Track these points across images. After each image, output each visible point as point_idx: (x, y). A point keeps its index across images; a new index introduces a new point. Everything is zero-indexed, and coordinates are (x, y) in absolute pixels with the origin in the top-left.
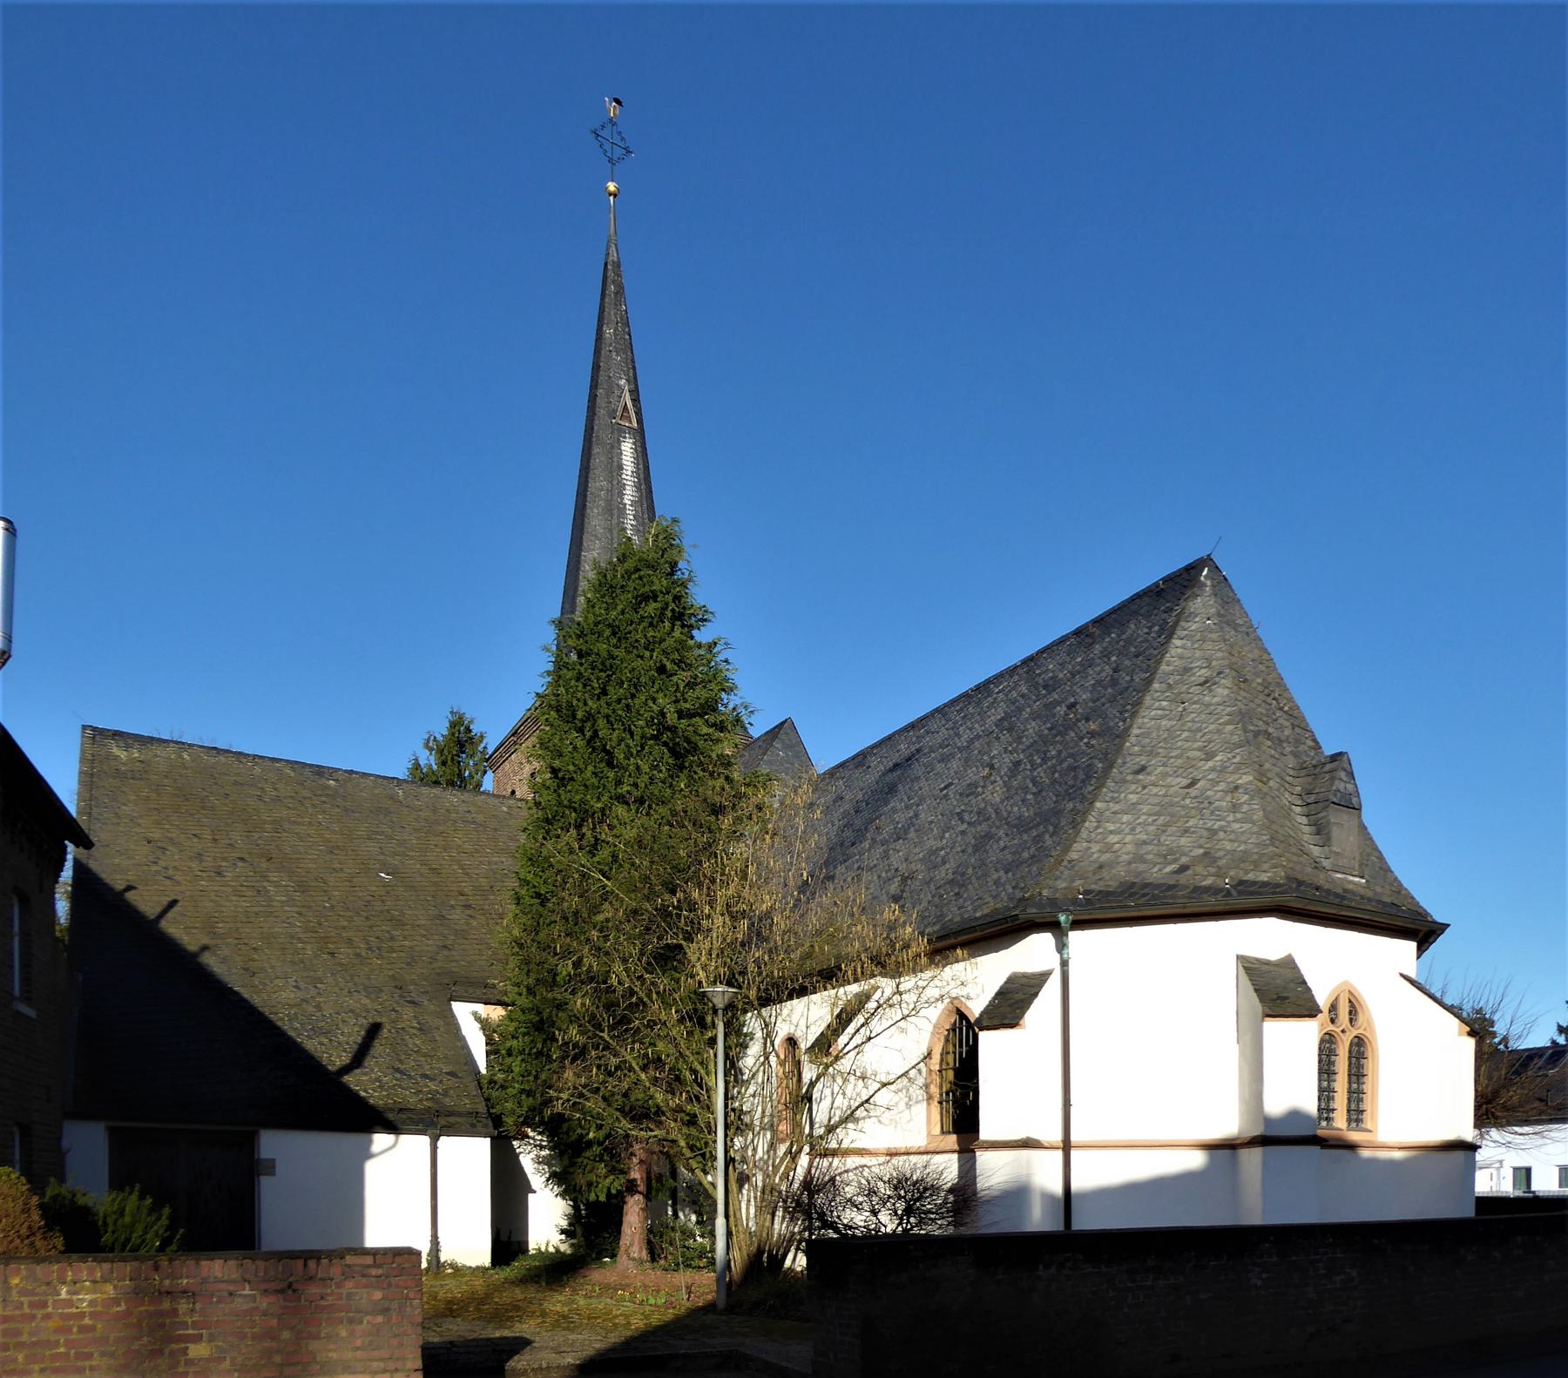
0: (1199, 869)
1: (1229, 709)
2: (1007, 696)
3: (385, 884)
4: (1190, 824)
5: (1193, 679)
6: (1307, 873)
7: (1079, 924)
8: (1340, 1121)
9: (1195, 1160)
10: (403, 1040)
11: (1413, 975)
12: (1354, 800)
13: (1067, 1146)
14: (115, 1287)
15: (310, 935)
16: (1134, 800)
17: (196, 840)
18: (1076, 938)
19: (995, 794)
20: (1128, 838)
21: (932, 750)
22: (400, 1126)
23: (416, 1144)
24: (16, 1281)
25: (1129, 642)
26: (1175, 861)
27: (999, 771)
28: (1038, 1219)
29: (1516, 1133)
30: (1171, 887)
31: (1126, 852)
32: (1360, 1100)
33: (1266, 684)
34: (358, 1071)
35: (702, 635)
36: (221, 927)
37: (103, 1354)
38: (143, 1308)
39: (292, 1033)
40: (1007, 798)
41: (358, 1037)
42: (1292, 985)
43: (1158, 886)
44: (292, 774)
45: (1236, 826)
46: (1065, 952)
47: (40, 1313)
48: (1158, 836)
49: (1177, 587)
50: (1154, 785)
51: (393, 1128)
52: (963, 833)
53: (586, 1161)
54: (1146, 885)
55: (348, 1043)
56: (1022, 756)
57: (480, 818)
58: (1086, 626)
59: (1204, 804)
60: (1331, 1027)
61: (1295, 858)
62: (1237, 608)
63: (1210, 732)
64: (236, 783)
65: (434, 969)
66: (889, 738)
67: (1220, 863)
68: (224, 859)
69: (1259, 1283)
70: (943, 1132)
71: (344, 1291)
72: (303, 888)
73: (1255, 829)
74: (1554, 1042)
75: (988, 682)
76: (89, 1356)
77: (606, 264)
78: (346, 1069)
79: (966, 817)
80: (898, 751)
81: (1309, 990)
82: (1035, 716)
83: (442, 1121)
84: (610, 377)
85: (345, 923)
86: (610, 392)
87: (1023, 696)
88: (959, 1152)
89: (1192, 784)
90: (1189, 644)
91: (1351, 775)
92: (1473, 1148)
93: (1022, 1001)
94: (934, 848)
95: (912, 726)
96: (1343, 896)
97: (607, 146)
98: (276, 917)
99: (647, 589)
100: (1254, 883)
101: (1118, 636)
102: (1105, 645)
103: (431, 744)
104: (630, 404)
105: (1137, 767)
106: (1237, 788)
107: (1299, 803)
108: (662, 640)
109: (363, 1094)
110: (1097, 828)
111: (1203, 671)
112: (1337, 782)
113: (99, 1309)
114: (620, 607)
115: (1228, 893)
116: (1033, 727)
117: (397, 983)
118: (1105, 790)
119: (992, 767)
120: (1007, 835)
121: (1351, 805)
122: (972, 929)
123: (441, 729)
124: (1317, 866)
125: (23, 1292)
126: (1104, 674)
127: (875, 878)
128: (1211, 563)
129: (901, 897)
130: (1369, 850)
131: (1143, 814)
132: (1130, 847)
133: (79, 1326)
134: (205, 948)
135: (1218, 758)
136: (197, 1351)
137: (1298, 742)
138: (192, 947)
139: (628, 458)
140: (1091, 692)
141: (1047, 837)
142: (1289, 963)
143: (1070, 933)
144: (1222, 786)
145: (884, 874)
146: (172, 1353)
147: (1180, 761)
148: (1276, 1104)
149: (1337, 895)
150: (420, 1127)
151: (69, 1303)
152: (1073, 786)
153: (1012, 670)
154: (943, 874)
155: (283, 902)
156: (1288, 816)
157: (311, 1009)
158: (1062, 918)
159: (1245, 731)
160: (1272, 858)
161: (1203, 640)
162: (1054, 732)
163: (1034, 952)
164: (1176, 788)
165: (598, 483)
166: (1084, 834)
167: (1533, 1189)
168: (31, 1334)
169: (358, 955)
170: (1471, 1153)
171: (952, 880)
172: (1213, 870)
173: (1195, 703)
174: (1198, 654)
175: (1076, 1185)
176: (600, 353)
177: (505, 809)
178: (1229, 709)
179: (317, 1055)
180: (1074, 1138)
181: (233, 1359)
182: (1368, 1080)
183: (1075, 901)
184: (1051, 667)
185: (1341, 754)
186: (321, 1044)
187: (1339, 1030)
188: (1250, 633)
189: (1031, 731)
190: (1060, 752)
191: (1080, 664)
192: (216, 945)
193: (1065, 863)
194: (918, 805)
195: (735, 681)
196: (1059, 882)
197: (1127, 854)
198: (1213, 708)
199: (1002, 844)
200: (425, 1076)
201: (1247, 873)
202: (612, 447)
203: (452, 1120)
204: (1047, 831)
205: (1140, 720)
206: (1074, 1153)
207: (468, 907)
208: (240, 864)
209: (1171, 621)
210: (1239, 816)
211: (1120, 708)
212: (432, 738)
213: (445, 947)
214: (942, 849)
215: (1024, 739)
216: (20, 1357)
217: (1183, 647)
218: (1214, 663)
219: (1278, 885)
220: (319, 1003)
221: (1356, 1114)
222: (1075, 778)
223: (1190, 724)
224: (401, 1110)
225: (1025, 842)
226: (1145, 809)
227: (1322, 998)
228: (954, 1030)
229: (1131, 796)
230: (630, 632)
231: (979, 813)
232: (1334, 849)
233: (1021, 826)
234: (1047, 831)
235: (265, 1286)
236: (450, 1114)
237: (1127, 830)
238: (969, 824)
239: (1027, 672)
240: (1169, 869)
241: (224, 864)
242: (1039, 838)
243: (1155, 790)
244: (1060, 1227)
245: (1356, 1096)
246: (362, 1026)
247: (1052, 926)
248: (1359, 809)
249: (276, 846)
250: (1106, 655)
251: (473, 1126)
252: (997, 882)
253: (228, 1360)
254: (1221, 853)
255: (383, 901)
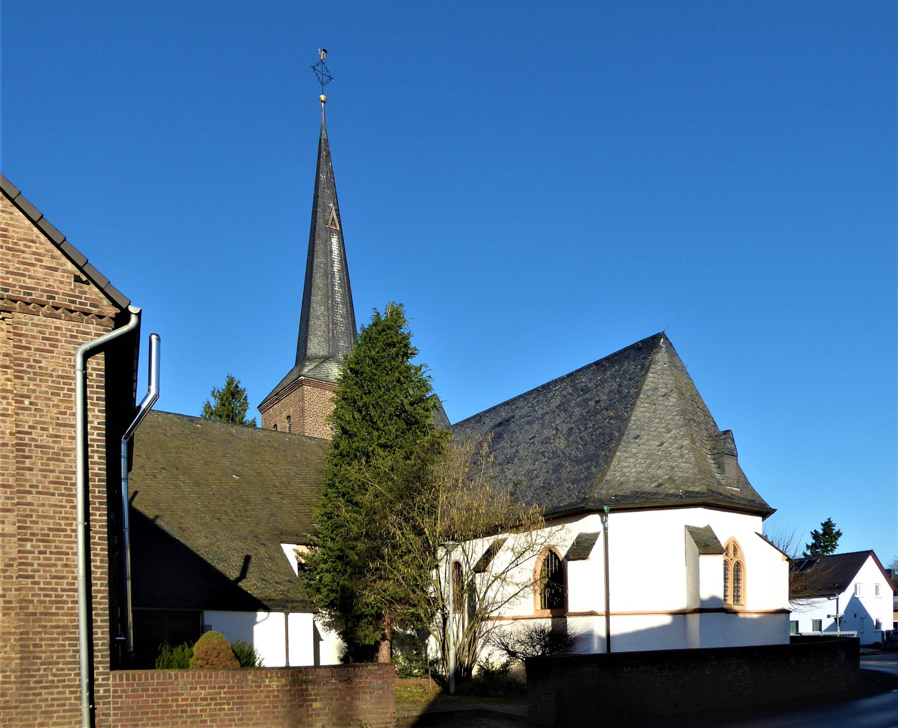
0: (667, 485)
1: (677, 409)
2: (560, 393)
3: (237, 482)
4: (661, 464)
5: (659, 393)
6: (715, 487)
7: (613, 511)
8: (730, 601)
9: (667, 620)
10: (262, 564)
11: (761, 533)
12: (735, 452)
13: (608, 614)
14: (286, 680)
15: (206, 509)
16: (635, 452)
17: (139, 458)
18: (612, 517)
19: (561, 443)
20: (633, 470)
21: (521, 417)
22: (270, 608)
23: (570, 620)
24: (250, 677)
25: (625, 371)
26: (656, 481)
27: (561, 432)
28: (597, 648)
29: (799, 604)
30: (655, 494)
31: (633, 476)
32: (738, 591)
33: (692, 396)
34: (244, 580)
35: (413, 362)
36: (163, 506)
37: (282, 706)
38: (296, 688)
39: (209, 561)
40: (568, 446)
41: (241, 563)
42: (711, 540)
43: (649, 493)
44: (178, 421)
45: (683, 465)
46: (606, 523)
47: (259, 690)
48: (647, 469)
49: (648, 347)
50: (644, 444)
51: (267, 609)
52: (546, 462)
53: (363, 624)
54: (644, 493)
55: (237, 566)
56: (573, 425)
57: (276, 445)
58: (601, 360)
59: (667, 455)
60: (726, 558)
61: (710, 480)
62: (677, 358)
63: (668, 419)
64: (151, 426)
65: (269, 527)
66: (494, 408)
67: (677, 482)
68: (155, 469)
69: (709, 673)
70: (542, 608)
71: (368, 681)
72: (197, 484)
73: (692, 467)
74: (805, 554)
75: (549, 384)
76: (277, 707)
77: (320, 140)
78: (239, 579)
79: (546, 454)
80: (501, 416)
81: (719, 541)
82: (579, 406)
83: (290, 605)
84: (324, 202)
85: (222, 503)
86: (324, 210)
87: (570, 394)
88: (552, 618)
89: (662, 444)
90: (656, 376)
91: (733, 441)
92: (787, 612)
93: (588, 547)
94: (530, 469)
95: (507, 403)
96: (731, 497)
97: (320, 75)
98: (188, 500)
99: (390, 340)
100: (693, 492)
101: (619, 368)
102: (612, 372)
103: (215, 394)
104: (335, 217)
105: (635, 436)
106: (682, 447)
107: (710, 453)
108: (399, 366)
109: (249, 592)
110: (618, 464)
111: (664, 389)
112: (727, 444)
113: (280, 688)
114: (377, 350)
115: (681, 497)
116: (577, 410)
117: (255, 535)
118: (620, 446)
119: (557, 430)
120: (570, 465)
121: (733, 455)
122: (555, 513)
123: (222, 386)
124: (719, 484)
125: (253, 681)
126: (613, 387)
127: (498, 483)
128: (663, 336)
129: (515, 493)
130: (740, 475)
131: (640, 458)
132: (634, 474)
133: (273, 695)
134: (157, 517)
135: (672, 432)
136: (316, 705)
137: (707, 423)
138: (151, 517)
139: (335, 247)
140: (608, 396)
141: (593, 468)
142: (708, 529)
143: (610, 515)
144: (675, 446)
145: (503, 481)
146: (307, 706)
147: (655, 433)
148: (705, 595)
149: (729, 497)
150: (280, 608)
151: (269, 686)
152: (603, 444)
153: (562, 379)
154: (538, 483)
155: (189, 491)
156: (705, 460)
157: (215, 549)
158: (605, 508)
159: (685, 419)
160: (700, 481)
161: (663, 374)
162: (589, 414)
163: (590, 524)
164: (654, 446)
165: (319, 260)
166: (612, 468)
167: (799, 632)
168: (256, 698)
169: (232, 520)
170: (787, 615)
171: (543, 486)
172: (674, 486)
173: (660, 405)
174: (661, 381)
175: (612, 633)
176: (318, 188)
177: (287, 439)
178: (677, 409)
179: (224, 572)
180: (611, 611)
181: (329, 708)
182: (742, 582)
183: (611, 500)
184: (584, 380)
185: (728, 431)
186: (224, 566)
187: (729, 559)
188: (683, 370)
189: (577, 412)
190: (594, 425)
191: (600, 380)
192: (162, 515)
193: (604, 481)
194: (518, 446)
195: (432, 386)
196: (602, 491)
197: (633, 477)
198: (669, 408)
199: (568, 469)
200: (276, 582)
201: (689, 487)
202: (327, 241)
203: (294, 604)
204: (592, 465)
205: (635, 413)
206: (611, 617)
207: (280, 493)
208: (164, 471)
209: (647, 364)
210: (684, 460)
211: (624, 405)
212: (216, 391)
213: (272, 515)
214: (535, 470)
215: (573, 417)
216: (253, 708)
217: (653, 377)
218: (669, 386)
219: (703, 493)
220: (219, 545)
221: (737, 598)
222: (604, 439)
223: (659, 415)
224: (269, 600)
225: (581, 470)
226: (640, 456)
227: (723, 544)
228: (548, 560)
229: (633, 450)
230: (383, 362)
231: (553, 453)
232: (726, 475)
233: (578, 461)
234: (592, 465)
235: (341, 679)
236: (293, 602)
237: (632, 466)
238: (548, 458)
239: (571, 382)
240: (653, 485)
241: (156, 471)
242: (588, 468)
243: (644, 447)
244: (605, 651)
245: (737, 589)
246: (241, 557)
247: (601, 512)
248: (737, 456)
249: (179, 461)
250: (613, 377)
251: (305, 607)
252: (569, 489)
253: (327, 709)
254: (677, 478)
255: (237, 491)
